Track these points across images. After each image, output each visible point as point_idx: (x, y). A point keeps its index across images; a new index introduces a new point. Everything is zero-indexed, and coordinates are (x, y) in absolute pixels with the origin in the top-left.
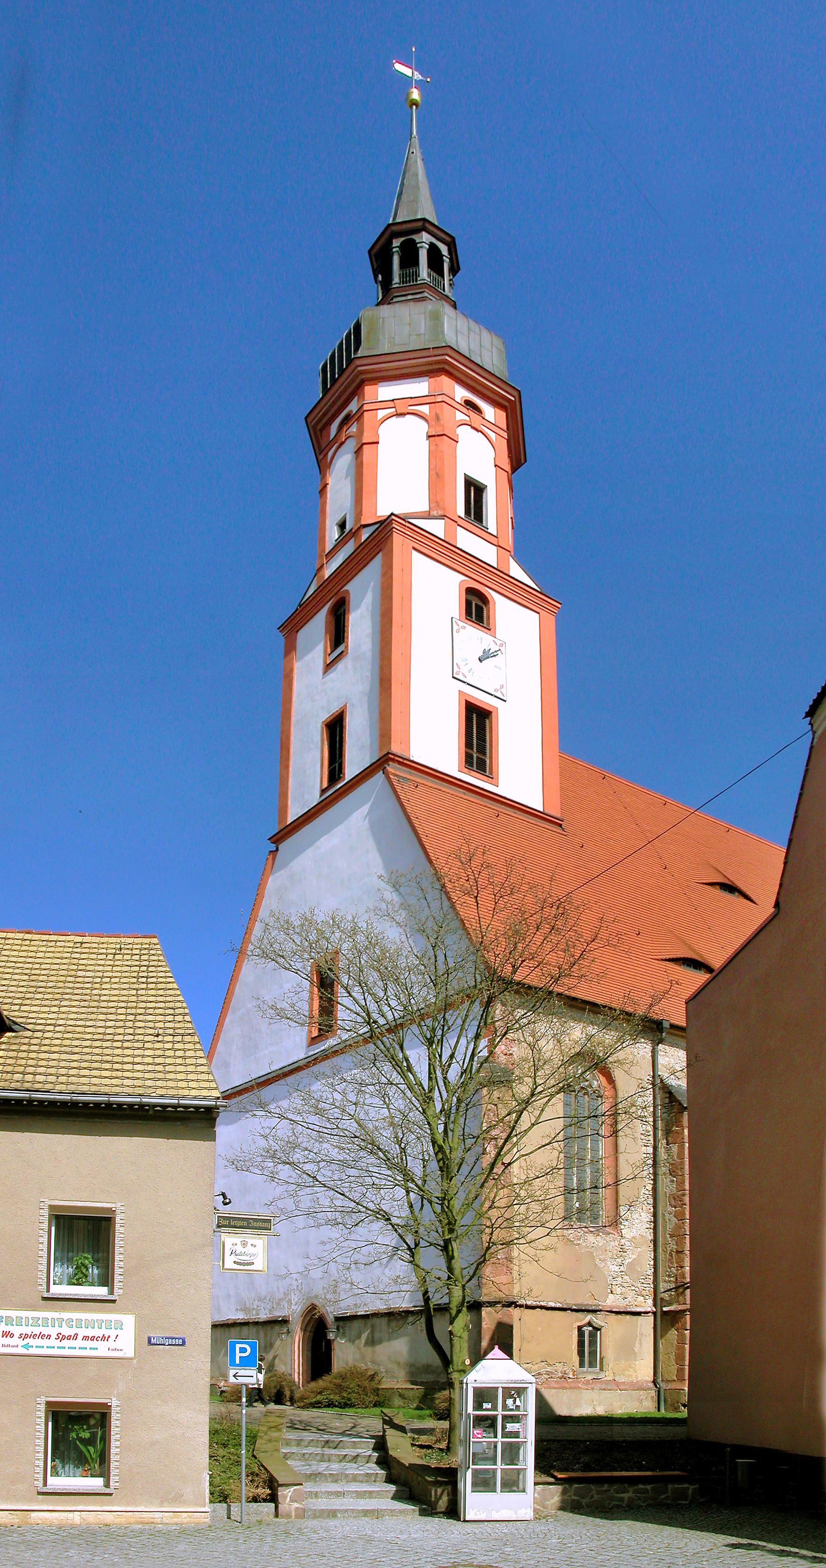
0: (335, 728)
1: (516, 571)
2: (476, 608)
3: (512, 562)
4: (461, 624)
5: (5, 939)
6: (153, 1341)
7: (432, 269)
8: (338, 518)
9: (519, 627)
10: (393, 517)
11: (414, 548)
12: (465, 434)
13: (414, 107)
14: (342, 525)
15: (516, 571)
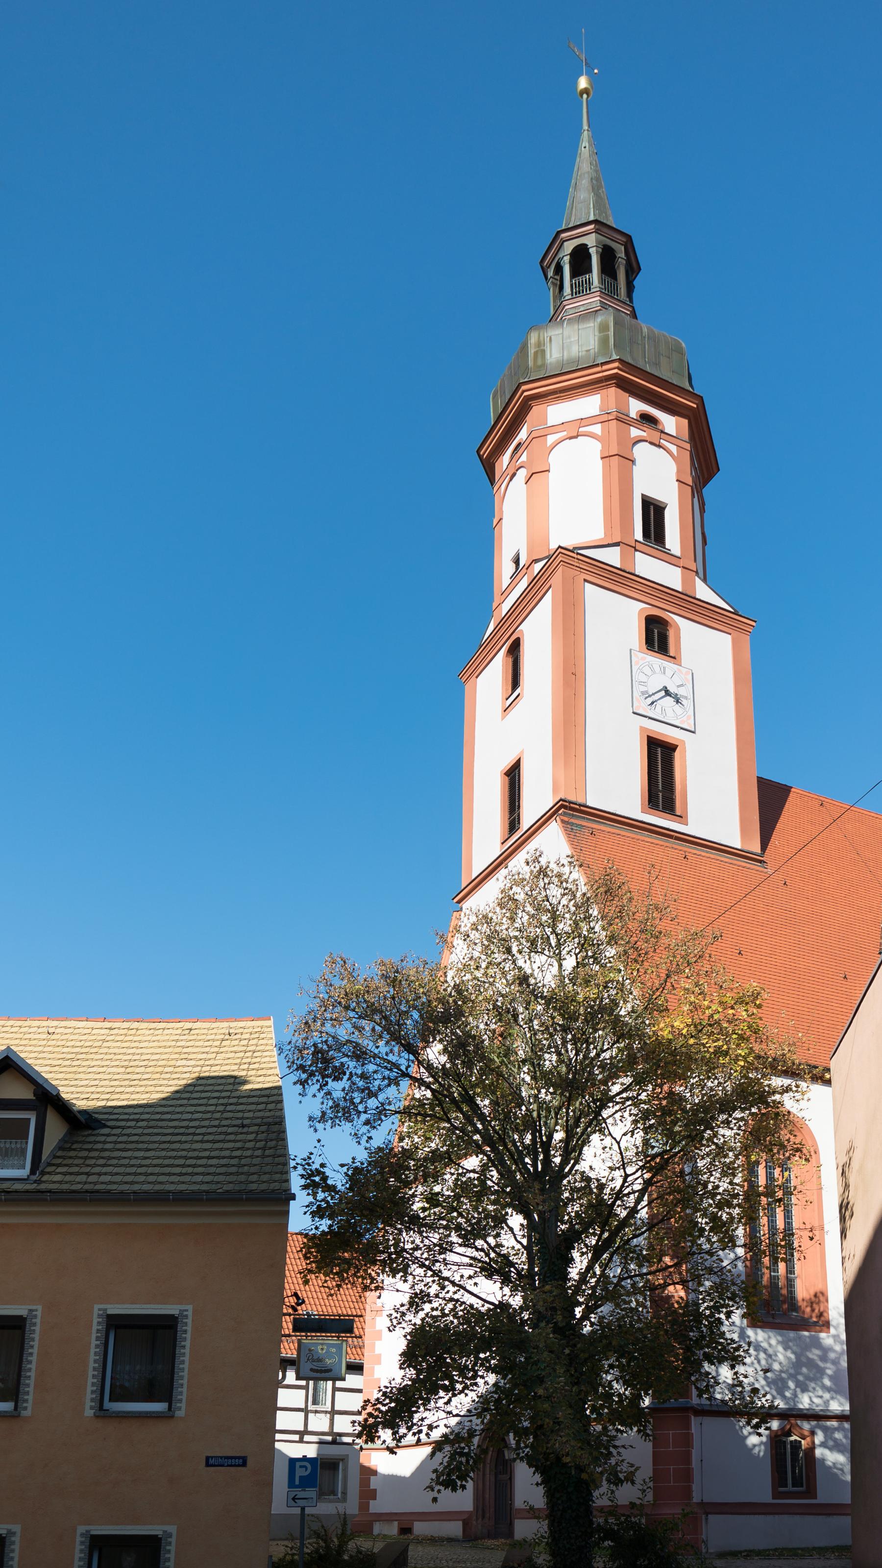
0: (513, 774)
1: (703, 592)
2: (657, 637)
3: (699, 583)
4: (641, 655)
5: (110, 1029)
6: (211, 1462)
7: (606, 274)
8: (512, 554)
9: (707, 653)
10: (560, 550)
11: (585, 580)
12: (642, 452)
13: (585, 96)
14: (517, 561)
15: (703, 592)
